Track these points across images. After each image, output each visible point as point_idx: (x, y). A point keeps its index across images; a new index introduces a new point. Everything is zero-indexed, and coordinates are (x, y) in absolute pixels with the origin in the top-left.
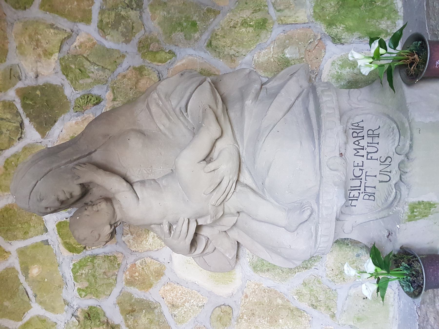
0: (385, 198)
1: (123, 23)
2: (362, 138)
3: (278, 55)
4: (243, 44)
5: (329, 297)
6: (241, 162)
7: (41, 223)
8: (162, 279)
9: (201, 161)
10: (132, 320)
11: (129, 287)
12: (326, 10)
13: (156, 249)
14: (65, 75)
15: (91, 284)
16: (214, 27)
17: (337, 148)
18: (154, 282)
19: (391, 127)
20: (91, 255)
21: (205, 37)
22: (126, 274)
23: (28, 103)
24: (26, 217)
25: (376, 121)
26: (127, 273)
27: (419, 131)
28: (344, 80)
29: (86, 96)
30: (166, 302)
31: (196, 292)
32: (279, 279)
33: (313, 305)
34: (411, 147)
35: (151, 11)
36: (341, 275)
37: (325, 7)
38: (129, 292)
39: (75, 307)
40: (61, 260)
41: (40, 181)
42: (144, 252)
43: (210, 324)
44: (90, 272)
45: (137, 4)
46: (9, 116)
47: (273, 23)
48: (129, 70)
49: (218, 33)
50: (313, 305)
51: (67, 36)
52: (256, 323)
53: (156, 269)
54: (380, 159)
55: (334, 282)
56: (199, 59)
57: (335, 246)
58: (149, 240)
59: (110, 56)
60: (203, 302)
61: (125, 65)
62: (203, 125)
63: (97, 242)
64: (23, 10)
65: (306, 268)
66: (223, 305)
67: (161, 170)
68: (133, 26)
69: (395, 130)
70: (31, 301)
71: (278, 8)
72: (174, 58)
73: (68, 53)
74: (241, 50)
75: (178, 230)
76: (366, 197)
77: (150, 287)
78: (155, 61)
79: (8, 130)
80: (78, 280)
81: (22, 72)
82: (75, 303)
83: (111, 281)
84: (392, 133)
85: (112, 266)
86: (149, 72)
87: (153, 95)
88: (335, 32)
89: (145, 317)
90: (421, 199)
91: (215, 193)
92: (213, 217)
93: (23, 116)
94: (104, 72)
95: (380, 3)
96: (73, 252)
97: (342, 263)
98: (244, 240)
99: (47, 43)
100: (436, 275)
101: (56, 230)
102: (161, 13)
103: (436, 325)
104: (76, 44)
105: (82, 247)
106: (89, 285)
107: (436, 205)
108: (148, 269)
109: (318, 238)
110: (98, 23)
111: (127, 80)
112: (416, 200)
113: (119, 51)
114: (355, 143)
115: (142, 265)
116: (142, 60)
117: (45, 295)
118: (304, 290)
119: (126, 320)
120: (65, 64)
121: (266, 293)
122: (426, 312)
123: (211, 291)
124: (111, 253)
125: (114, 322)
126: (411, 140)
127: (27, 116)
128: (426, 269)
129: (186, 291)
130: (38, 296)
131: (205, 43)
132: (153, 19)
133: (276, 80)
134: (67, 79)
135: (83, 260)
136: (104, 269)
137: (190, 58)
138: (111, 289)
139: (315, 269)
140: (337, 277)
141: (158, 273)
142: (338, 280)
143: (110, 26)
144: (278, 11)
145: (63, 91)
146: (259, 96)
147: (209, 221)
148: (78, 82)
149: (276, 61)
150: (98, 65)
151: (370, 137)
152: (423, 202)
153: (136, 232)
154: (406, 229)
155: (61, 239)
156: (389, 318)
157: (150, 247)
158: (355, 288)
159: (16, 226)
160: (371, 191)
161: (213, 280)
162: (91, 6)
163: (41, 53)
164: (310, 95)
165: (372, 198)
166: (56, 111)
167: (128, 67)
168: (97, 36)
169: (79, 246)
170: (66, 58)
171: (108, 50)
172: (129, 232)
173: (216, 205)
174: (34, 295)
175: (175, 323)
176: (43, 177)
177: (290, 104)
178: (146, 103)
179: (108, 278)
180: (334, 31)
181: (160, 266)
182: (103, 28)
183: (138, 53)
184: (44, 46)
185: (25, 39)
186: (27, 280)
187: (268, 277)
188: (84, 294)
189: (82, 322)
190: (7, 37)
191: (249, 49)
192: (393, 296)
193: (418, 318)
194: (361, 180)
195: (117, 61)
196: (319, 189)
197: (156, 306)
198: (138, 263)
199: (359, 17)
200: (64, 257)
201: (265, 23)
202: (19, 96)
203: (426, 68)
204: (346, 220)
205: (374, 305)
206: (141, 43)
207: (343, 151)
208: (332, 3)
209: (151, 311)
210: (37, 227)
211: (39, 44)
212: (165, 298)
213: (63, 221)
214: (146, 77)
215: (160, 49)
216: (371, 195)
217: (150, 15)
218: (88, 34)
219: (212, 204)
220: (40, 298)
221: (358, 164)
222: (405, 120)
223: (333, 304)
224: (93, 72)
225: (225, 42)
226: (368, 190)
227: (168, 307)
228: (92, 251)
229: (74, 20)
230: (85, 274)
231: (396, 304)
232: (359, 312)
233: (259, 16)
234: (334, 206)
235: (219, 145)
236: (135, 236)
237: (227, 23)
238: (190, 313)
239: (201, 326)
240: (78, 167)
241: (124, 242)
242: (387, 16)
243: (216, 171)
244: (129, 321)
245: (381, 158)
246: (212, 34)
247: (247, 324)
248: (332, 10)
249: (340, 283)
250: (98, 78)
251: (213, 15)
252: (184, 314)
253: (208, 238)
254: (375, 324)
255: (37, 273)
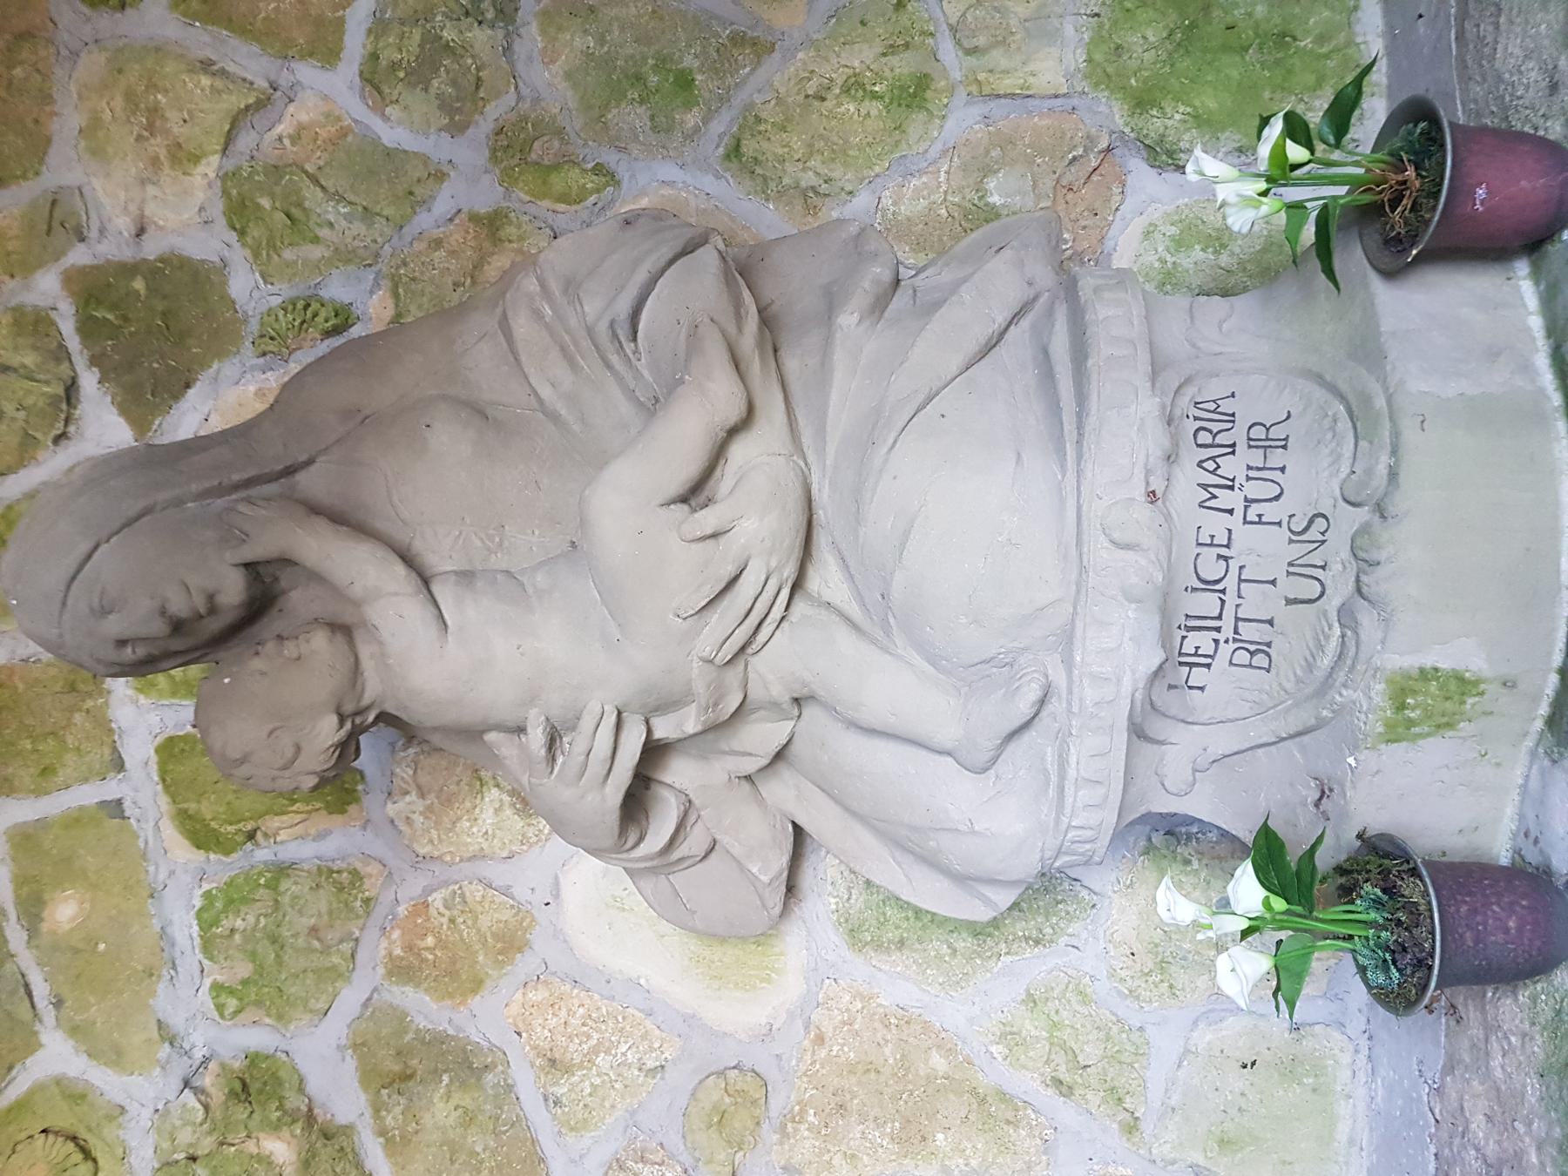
0: (1306, 660)
1: (445, 66)
2: (1230, 450)
3: (964, 198)
5: (1117, 1055)
7: (105, 738)
10: (398, 1110)
11: (397, 985)
12: (1130, 57)
14: (235, 229)
15: (260, 969)
16: (752, 95)
18: (490, 972)
19: (1330, 413)
21: (718, 126)
22: (389, 938)
26: (396, 934)
29: (302, 302)
30: (528, 1048)
32: (941, 980)
34: (1393, 475)
35: (543, 32)
36: (1161, 974)
37: (1126, 45)
39: (198, 1055)
40: (162, 876)
41: (106, 545)
42: (461, 861)
43: (684, 1137)
44: (261, 925)
46: (29, 359)
47: (951, 90)
48: (456, 225)
49: (763, 115)
51: (254, 99)
53: (501, 925)
54: (1289, 523)
55: (1137, 998)
56: (696, 196)
57: (1143, 868)
58: (483, 816)
60: (662, 1053)
61: (443, 205)
63: (287, 773)
64: (114, 9)
65: (1037, 942)
66: (734, 1068)
68: (479, 79)
69: (1339, 424)
71: (967, 44)
72: (610, 189)
73: (252, 157)
75: (580, 746)
76: (1242, 657)
78: (544, 196)
79: (24, 408)
82: (199, 1039)
83: (336, 959)
84: (1329, 436)
86: (522, 231)
90: (1428, 661)
91: (714, 617)
94: (370, 226)
95: (1309, 40)
96: (207, 849)
97: (1166, 929)
98: (820, 819)
99: (185, 121)
101: (155, 767)
102: (577, 42)
103: (1491, 1142)
104: (283, 130)
106: (255, 971)
107: (1482, 686)
109: (1066, 789)
110: (361, 64)
113: (425, 160)
114: (1204, 465)
117: (92, 1000)
118: (1028, 1025)
119: (377, 1109)
120: (239, 194)
121: (890, 1030)
122: (1462, 1099)
123: (694, 1016)
124: (343, 859)
125: (333, 1115)
126: (1394, 452)
127: (94, 361)
131: (718, 146)
132: (549, 58)
133: (947, 265)
134: (243, 245)
135: (241, 880)
136: (312, 916)
137: (666, 191)
139: (1070, 948)
140: (1147, 981)
141: (507, 939)
142: (1151, 991)
143: (402, 74)
144: (972, 51)
145: (224, 283)
146: (886, 307)
148: (279, 256)
149: (956, 215)
150: (350, 203)
151: (1257, 447)
152: (1436, 670)
155: (169, 800)
156: (1336, 1144)
157: (485, 846)
158: (1210, 1025)
161: (702, 973)
162: (344, 9)
163: (163, 153)
165: (1260, 660)
166: (195, 350)
167: (454, 211)
168: (355, 108)
169: (230, 828)
171: (389, 153)
172: (414, 786)
175: (556, 1129)
176: (117, 533)
177: (991, 331)
178: (499, 311)
180: (1155, 125)
184: (176, 130)
186: (34, 943)
187: (899, 969)
188: (232, 1004)
190: (51, 96)
193: (1433, 1130)
194: (1224, 594)
195: (418, 190)
196: (1075, 613)
197: (489, 1060)
198: (437, 899)
200: (172, 868)
201: (924, 90)
202: (72, 294)
203: (1440, 207)
206: (503, 136)
207: (1158, 485)
208: (1150, 34)
209: (473, 1080)
210: (90, 752)
211: (158, 123)
212: (524, 1035)
213: (181, 733)
214: (511, 245)
218: (326, 98)
219: (704, 654)
222: (1375, 388)
224: (331, 225)
225: (784, 146)
226: (1247, 631)
229: (285, 52)
230: (245, 930)
231: (1361, 1092)
233: (903, 66)
235: (740, 451)
236: (432, 803)
237: (797, 84)
238: (613, 1093)
240: (242, 508)
241: (392, 821)
243: (723, 540)
244: (389, 1112)
245: (1293, 519)
246: (745, 118)
248: (1149, 56)
249: (1156, 1004)
251: (749, 54)
252: (590, 1095)
253: (690, 801)
254: (1284, 1162)
255: (73, 919)
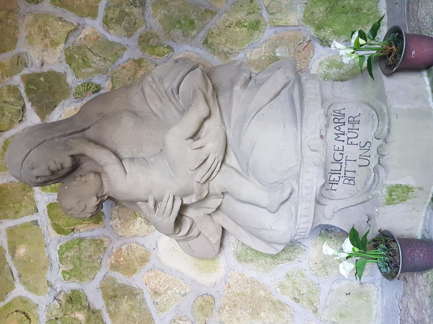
0: (364, 182)
2: (343, 124)
3: (269, 54)
4: (237, 43)
6: (228, 144)
8: (147, 266)
9: (189, 139)
10: (113, 306)
11: (113, 271)
12: (316, 15)
13: (143, 235)
15: (75, 267)
17: (318, 131)
19: (371, 114)
20: (79, 238)
21: (201, 35)
22: (111, 258)
23: (31, 88)
24: (19, 196)
25: (357, 109)
26: (113, 257)
27: (397, 116)
28: (331, 80)
29: (87, 84)
30: (149, 289)
31: (179, 279)
33: (295, 299)
34: (389, 131)
35: (153, 9)
36: (324, 269)
37: (314, 12)
38: (113, 277)
39: (58, 290)
40: (48, 241)
41: (33, 150)
42: (131, 237)
43: (192, 313)
44: (76, 255)
45: (140, 3)
46: (12, 100)
47: (266, 24)
49: (214, 32)
50: (295, 299)
52: (238, 315)
53: (142, 255)
54: (360, 144)
56: (195, 54)
57: (319, 240)
58: (137, 225)
59: (112, 49)
61: (126, 57)
62: (193, 104)
63: (83, 213)
64: (35, 3)
65: (289, 260)
66: (206, 294)
67: (151, 149)
68: (135, 22)
69: (374, 117)
70: (15, 281)
71: (270, 12)
74: (234, 48)
75: (163, 206)
77: (134, 273)
78: (153, 54)
79: (11, 113)
80: (63, 262)
81: (29, 59)
82: (59, 286)
83: (96, 264)
85: (98, 249)
87: (148, 78)
88: (324, 35)
89: (127, 303)
90: (399, 182)
92: (198, 196)
93: (26, 100)
94: (105, 62)
97: (325, 256)
98: (229, 226)
99: (55, 34)
100: (413, 256)
101: (47, 211)
102: (162, 12)
104: (82, 36)
105: (70, 229)
106: (74, 268)
107: (413, 190)
108: (133, 254)
109: (298, 218)
111: (126, 70)
112: (394, 183)
113: (120, 44)
114: (336, 128)
115: (127, 250)
116: (142, 53)
117: (29, 275)
119: (107, 305)
120: (69, 54)
127: (30, 100)
128: (403, 249)
129: (170, 278)
130: (23, 276)
131: (201, 40)
132: (154, 16)
136: (89, 252)
137: (187, 53)
138: (95, 272)
140: (320, 271)
143: (114, 21)
144: (271, 14)
145: (65, 78)
147: (194, 200)
148: (80, 71)
149: (267, 59)
150: (100, 56)
151: (351, 123)
152: (401, 185)
153: (124, 217)
154: (384, 213)
155: (50, 220)
157: (137, 233)
159: (8, 205)
160: (351, 175)
163: (49, 43)
164: (295, 84)
165: (352, 182)
167: (128, 59)
168: (101, 30)
169: (67, 228)
170: (71, 49)
171: (110, 43)
173: (201, 182)
174: (19, 275)
175: (157, 311)
176: (36, 147)
177: (277, 91)
179: (93, 262)
180: (322, 34)
181: (145, 252)
182: (107, 23)
183: (138, 46)
184: (52, 36)
185: (34, 30)
186: (13, 259)
187: (251, 267)
188: (68, 276)
189: (64, 306)
191: (242, 47)
192: (376, 293)
193: (399, 312)
194: (342, 164)
195: (118, 53)
196: (300, 169)
197: (138, 292)
198: (124, 248)
199: (346, 23)
201: (258, 24)
202: (24, 82)
203: (402, 56)
204: (327, 204)
205: (357, 302)
207: (323, 134)
208: (321, 9)
209: (134, 298)
211: (47, 35)
212: (148, 285)
213: (54, 202)
215: (159, 44)
216: (351, 180)
217: (152, 13)
218: (93, 28)
220: (24, 279)
221: (338, 148)
222: (384, 107)
223: (315, 299)
224: (95, 63)
225: (220, 40)
226: (348, 174)
227: (150, 294)
228: (80, 233)
230: (71, 256)
231: (379, 302)
232: (341, 308)
233: (252, 18)
234: (314, 185)
235: (207, 125)
236: (123, 221)
238: (172, 301)
239: (182, 315)
241: (112, 226)
242: (372, 22)
243: (202, 149)
244: (111, 306)
246: (208, 33)
247: (229, 315)
248: (320, 15)
250: (99, 68)
252: (166, 301)
253: (193, 221)
254: (358, 321)
255: (24, 253)
